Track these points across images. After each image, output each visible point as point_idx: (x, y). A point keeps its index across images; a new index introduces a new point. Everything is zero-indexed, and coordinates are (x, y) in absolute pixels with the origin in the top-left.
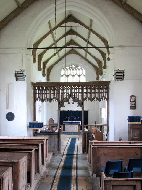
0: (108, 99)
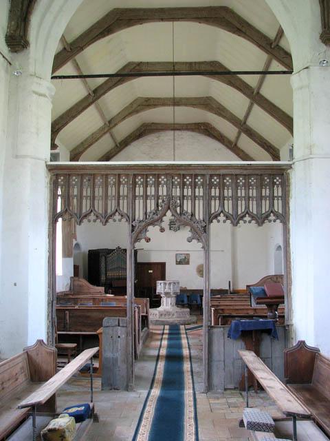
0: (284, 218)
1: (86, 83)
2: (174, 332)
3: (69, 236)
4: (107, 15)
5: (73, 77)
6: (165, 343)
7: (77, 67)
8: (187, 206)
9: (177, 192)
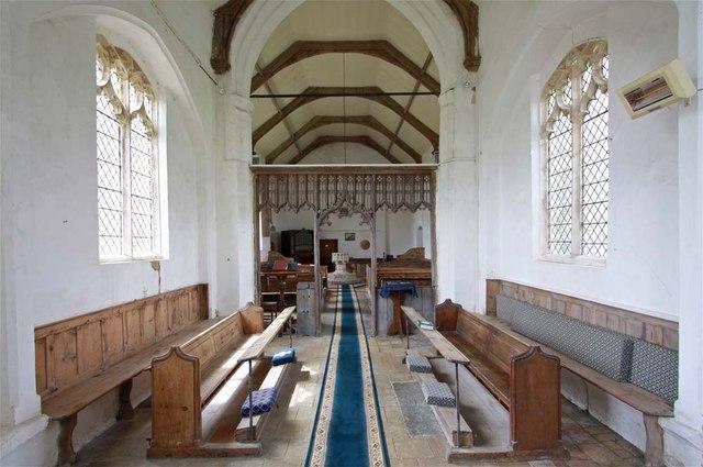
0: (431, 207)
1: (276, 104)
2: (346, 288)
3: (267, 221)
4: (291, 47)
5: (263, 96)
6: (340, 298)
7: (270, 90)
8: (359, 199)
9: (350, 188)
